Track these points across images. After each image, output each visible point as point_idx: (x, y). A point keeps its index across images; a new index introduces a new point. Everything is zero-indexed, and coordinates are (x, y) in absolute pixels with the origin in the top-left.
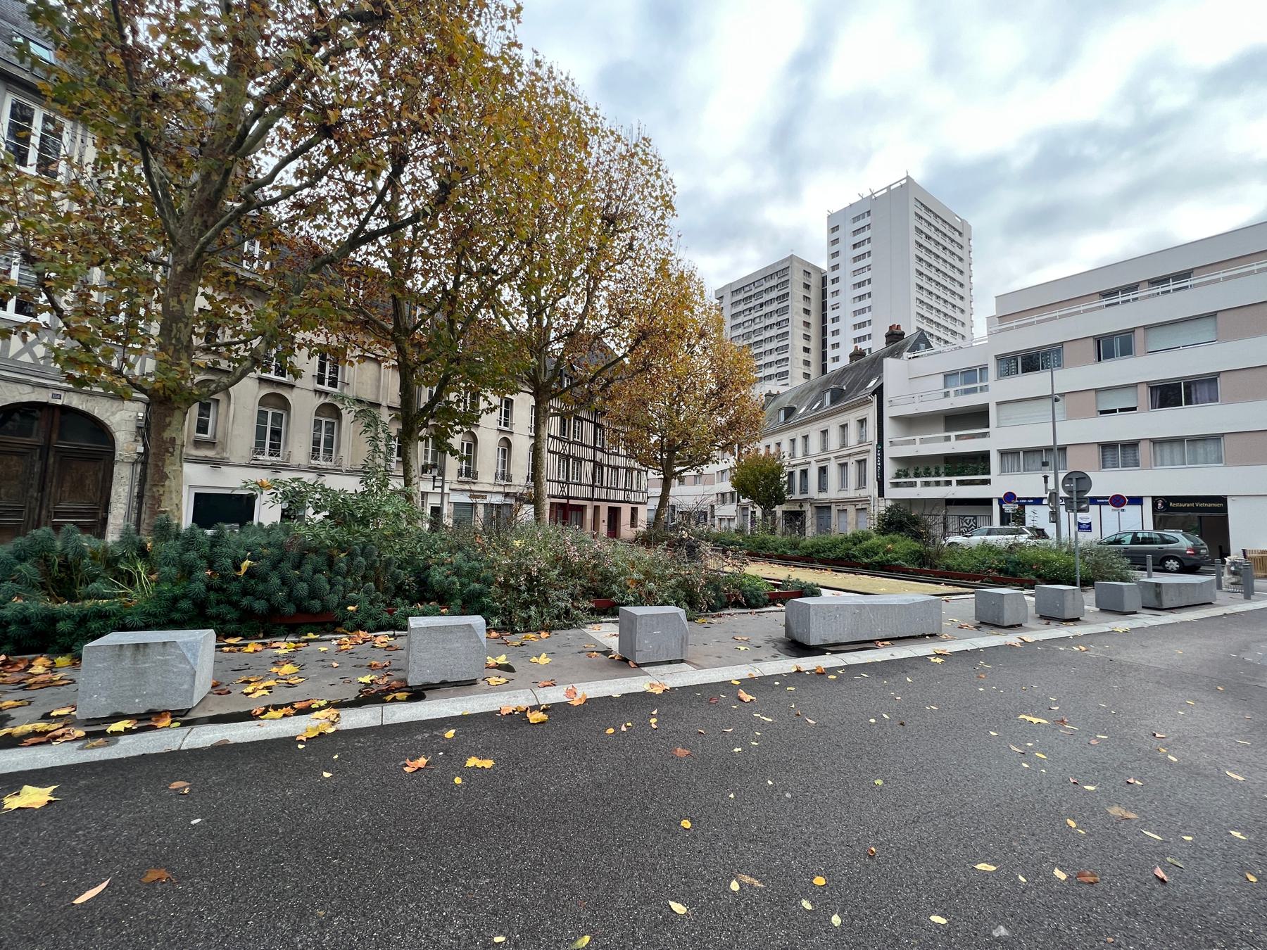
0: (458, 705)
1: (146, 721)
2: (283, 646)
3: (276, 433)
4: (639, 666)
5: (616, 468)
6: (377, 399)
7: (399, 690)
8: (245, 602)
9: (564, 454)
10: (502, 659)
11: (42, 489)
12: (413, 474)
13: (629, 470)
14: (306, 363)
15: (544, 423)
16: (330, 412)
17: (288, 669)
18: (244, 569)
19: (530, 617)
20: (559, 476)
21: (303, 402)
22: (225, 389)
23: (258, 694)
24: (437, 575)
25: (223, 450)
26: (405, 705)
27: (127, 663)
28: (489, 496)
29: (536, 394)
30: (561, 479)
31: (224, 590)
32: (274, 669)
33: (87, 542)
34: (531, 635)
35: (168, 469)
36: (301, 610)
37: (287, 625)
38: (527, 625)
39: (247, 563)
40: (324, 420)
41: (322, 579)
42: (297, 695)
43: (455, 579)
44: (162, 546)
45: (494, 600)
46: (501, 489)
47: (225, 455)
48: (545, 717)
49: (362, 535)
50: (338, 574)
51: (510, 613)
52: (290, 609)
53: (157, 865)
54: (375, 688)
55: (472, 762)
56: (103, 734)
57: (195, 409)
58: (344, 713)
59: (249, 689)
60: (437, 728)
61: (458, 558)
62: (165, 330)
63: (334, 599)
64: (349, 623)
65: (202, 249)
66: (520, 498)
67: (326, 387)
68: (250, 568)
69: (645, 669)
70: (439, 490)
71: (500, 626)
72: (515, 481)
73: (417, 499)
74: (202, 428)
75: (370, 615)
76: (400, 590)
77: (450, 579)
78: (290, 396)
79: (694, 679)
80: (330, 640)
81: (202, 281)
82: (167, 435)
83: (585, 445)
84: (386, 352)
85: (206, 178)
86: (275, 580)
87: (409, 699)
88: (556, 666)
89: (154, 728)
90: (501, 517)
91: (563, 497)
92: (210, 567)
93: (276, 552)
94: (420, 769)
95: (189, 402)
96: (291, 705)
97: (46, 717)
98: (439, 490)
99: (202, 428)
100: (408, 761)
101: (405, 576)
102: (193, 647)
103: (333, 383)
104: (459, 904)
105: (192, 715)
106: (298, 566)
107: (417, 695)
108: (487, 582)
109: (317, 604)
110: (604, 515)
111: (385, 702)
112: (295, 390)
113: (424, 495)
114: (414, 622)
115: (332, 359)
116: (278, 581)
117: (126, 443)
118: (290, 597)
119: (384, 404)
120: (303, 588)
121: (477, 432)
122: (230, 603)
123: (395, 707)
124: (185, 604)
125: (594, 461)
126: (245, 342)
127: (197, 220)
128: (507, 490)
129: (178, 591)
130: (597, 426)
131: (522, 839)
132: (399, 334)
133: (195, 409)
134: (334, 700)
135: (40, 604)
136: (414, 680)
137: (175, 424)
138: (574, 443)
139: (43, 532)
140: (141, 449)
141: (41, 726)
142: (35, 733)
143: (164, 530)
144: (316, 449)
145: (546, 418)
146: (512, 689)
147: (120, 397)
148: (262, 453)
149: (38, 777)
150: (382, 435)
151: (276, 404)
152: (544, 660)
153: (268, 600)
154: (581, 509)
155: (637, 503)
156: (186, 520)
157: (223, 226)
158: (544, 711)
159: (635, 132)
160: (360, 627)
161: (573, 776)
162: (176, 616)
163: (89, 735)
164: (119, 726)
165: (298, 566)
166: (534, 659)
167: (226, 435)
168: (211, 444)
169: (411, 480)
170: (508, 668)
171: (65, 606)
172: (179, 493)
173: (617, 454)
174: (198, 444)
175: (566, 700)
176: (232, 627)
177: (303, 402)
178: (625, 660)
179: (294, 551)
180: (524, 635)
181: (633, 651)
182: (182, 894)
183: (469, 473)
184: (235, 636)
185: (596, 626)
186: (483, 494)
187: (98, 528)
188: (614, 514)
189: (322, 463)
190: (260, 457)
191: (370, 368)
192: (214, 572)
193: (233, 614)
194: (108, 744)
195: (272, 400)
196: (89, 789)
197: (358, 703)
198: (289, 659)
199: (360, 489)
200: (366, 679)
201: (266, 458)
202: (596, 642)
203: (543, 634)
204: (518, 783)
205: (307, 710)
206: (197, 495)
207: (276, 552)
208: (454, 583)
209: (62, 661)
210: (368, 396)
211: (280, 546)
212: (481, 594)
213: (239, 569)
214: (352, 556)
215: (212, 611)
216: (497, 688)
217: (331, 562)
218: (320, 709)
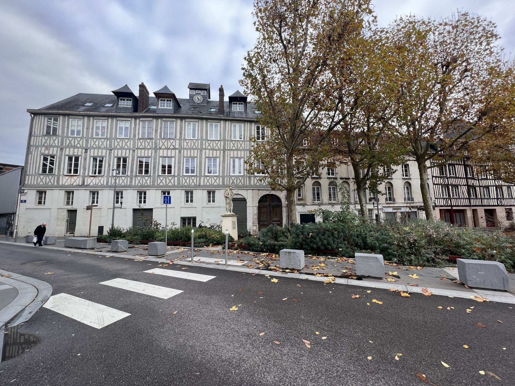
0: (374, 284)
1: (292, 270)
2: (322, 259)
3: (318, 194)
4: (471, 288)
5: (487, 187)
6: (348, 176)
7: (354, 276)
8: (311, 245)
9: (444, 184)
10: (395, 273)
11: (270, 215)
12: (363, 203)
13: (499, 187)
14: (324, 172)
15: (425, 172)
16: (332, 184)
17: (323, 265)
18: (310, 236)
19: (412, 260)
20: (443, 195)
21: (325, 182)
22: (303, 183)
23: (315, 270)
24: (369, 240)
25: (305, 201)
26: (355, 280)
27: (287, 256)
28: (402, 208)
29: (417, 160)
30: (445, 197)
31: (306, 241)
32: (319, 264)
33: (279, 228)
34: (412, 267)
35: (293, 208)
36: (326, 249)
37: (323, 253)
38: (411, 263)
39: (311, 234)
40: (331, 187)
41: (330, 239)
42: (325, 272)
43: (376, 242)
44: (292, 229)
45: (394, 251)
46: (408, 205)
47: (306, 202)
48: (409, 296)
49: (341, 225)
50: (335, 238)
51: (402, 257)
52: (323, 248)
53: (295, 298)
54: (347, 274)
55: (374, 301)
56: (285, 272)
57: (297, 190)
58: (336, 278)
59: (313, 268)
60: (365, 289)
61: (377, 234)
62: (288, 171)
63: (335, 246)
64: (340, 254)
65: (293, 148)
66: (420, 208)
67: (331, 176)
68: (312, 235)
69: (476, 290)
70: (376, 208)
71: (397, 261)
72: (416, 200)
73: (367, 212)
74: (299, 195)
75: (346, 252)
76: (357, 245)
77: (374, 241)
78: (321, 181)
79: (511, 301)
80: (335, 259)
81: (294, 155)
82: (291, 199)
83: (459, 178)
84: (347, 160)
85: (291, 128)
86: (318, 239)
87: (357, 279)
88: (421, 280)
89: (293, 272)
90: (408, 216)
91: (448, 206)
92: (303, 235)
93: (318, 231)
94: (356, 298)
95: (295, 189)
96: (323, 274)
97: (276, 266)
98: (376, 208)
99: (299, 195)
100: (353, 295)
101: (359, 241)
102: (299, 254)
103: (333, 174)
104: (361, 331)
105: (301, 272)
106: (323, 235)
107: (360, 278)
108: (391, 244)
109: (330, 247)
110: (481, 213)
111: (349, 278)
112: (322, 179)
113: (370, 210)
114: (356, 254)
115: (331, 167)
116: (319, 239)
117: (284, 202)
118: (322, 244)
119: (351, 178)
120: (325, 242)
121: (392, 182)
122: (308, 245)
123: (352, 280)
124: (298, 244)
125: (467, 185)
126: (305, 169)
127: (291, 140)
128: (412, 205)
129: (296, 241)
130: (466, 166)
131: (386, 325)
132: (351, 152)
133: (297, 190)
134: (334, 275)
135: (272, 242)
136: (359, 273)
137: (293, 196)
138: (450, 177)
139: (271, 225)
140: (287, 203)
141: (275, 268)
142: (274, 269)
143: (292, 225)
144: (330, 197)
145: (425, 171)
146: (397, 284)
147: (282, 191)
148: (315, 200)
149: (276, 277)
150: (346, 192)
151: (317, 184)
152: (415, 276)
153: (317, 245)
154: (463, 212)
155: (476, 206)
156: (298, 221)
157: (297, 138)
158: (409, 294)
159: (457, 14)
160: (343, 256)
161: (414, 315)
162: (297, 247)
163: (283, 271)
164: (287, 271)
165: (323, 235)
166: (410, 276)
167: (305, 196)
168: (302, 200)
169: (363, 205)
170: (398, 277)
171: (276, 243)
172: (295, 214)
173: (487, 179)
174: (299, 200)
175: (422, 292)
176: (309, 252)
177: (325, 182)
178: (463, 284)
179: (322, 231)
180: (408, 267)
181: (466, 280)
182: (299, 305)
183: (391, 199)
184: (310, 254)
185: (451, 268)
186: (399, 208)
187: (281, 225)
188: (490, 213)
189: (333, 202)
190: (315, 202)
191: (343, 166)
192: (303, 236)
193: (309, 248)
194: (286, 274)
195: (316, 184)
196: (283, 282)
197: (341, 277)
198: (324, 262)
199: (341, 210)
200: (344, 271)
201: (316, 202)
202: (448, 275)
203: (419, 268)
204: (390, 311)
205: (327, 276)
206: (301, 215)
207: (318, 231)
208: (376, 243)
209: (277, 255)
210: (345, 176)
211: (318, 229)
212: (387, 248)
213: (309, 236)
214: (339, 233)
215: (304, 247)
216: (391, 282)
217: (333, 234)
218: (330, 276)
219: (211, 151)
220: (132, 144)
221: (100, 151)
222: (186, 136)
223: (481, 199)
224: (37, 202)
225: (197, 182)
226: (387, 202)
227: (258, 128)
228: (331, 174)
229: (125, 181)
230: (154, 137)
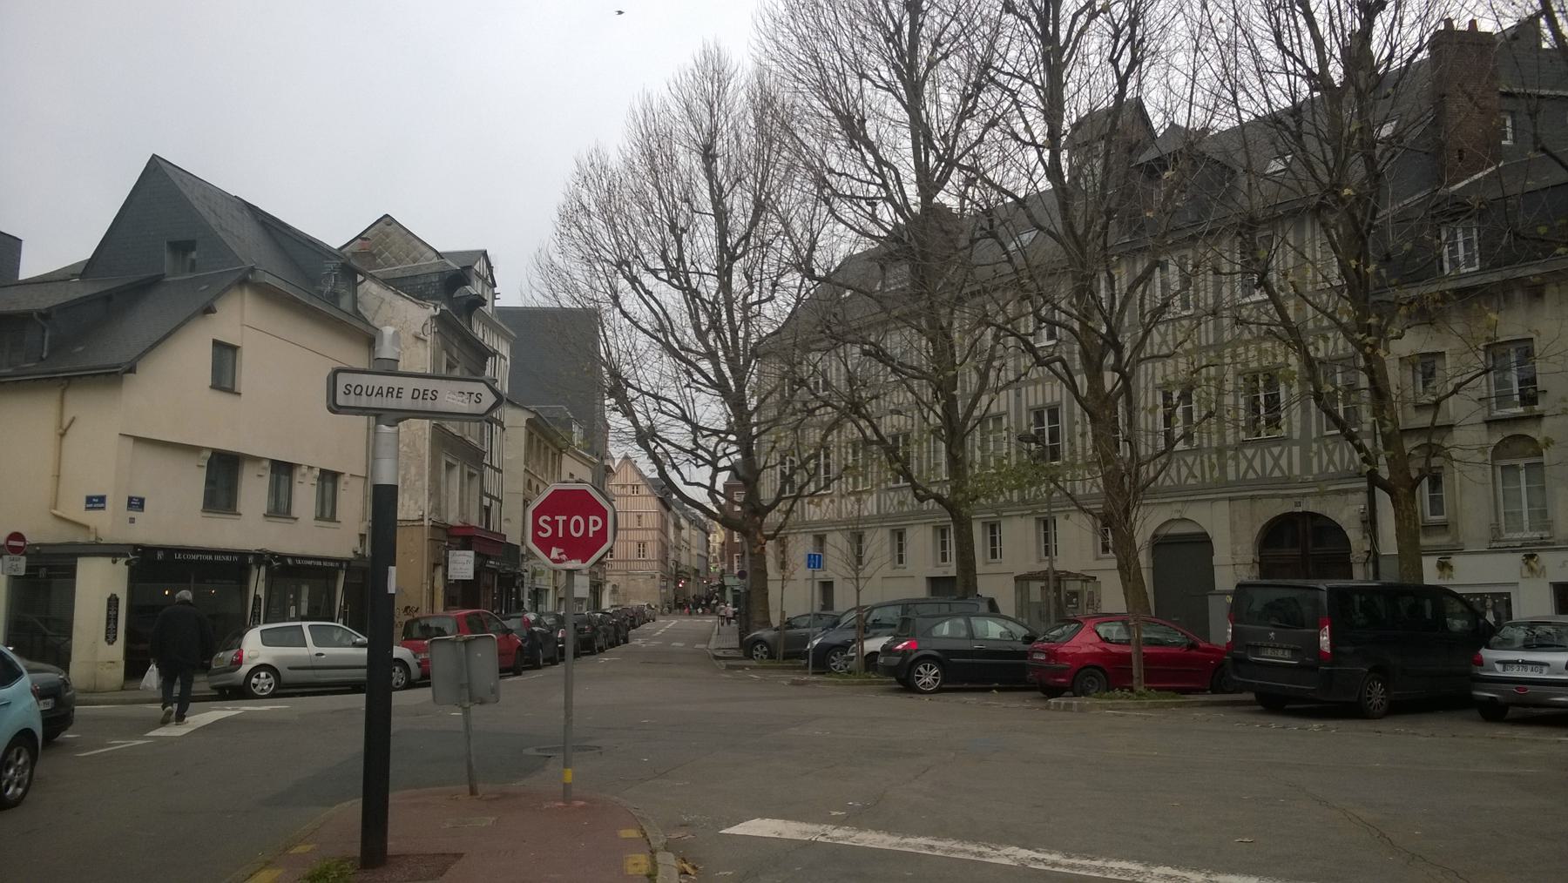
225: (885, 500)
229: (1284, 462)
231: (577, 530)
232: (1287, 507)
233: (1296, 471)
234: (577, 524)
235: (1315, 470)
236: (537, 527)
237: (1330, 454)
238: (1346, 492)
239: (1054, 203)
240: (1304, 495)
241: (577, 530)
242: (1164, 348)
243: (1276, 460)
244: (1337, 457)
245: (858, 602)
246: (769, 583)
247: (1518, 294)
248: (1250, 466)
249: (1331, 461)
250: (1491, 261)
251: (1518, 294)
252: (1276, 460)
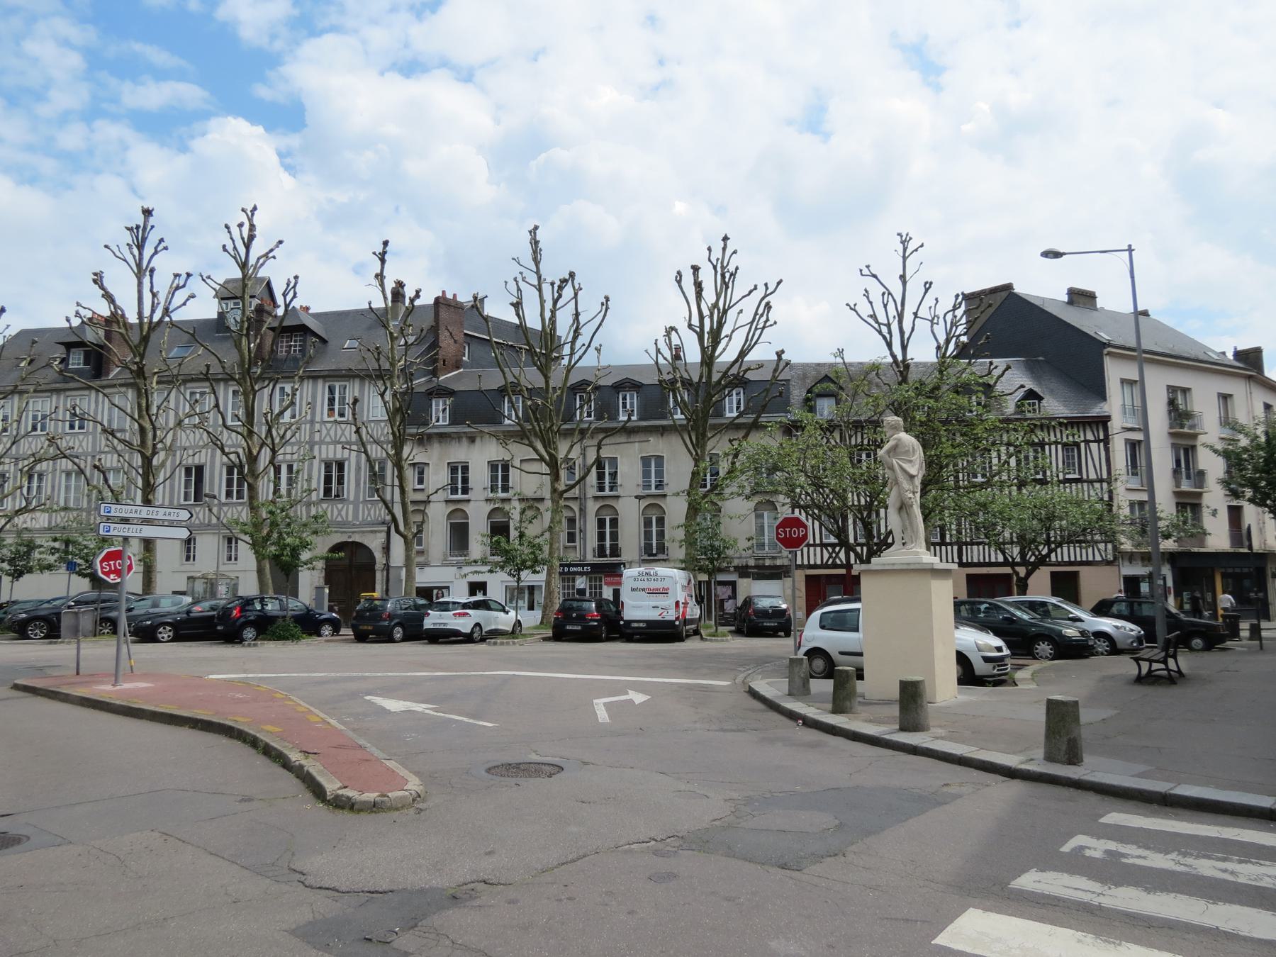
78: (468, 508)
91: (835, 566)
112: (472, 503)
219: (331, 447)
220: (90, 445)
221: (324, 447)
222: (371, 414)
223: (960, 544)
224: (184, 559)
225: (204, 518)
226: (642, 558)
227: (331, 391)
228: (460, 491)
229: (343, 513)
230: (128, 428)
231: (795, 534)
232: (344, 538)
233: (350, 519)
234: (795, 531)
235: (361, 519)
236: (778, 534)
237: (369, 510)
238: (376, 532)
239: (223, 289)
240: (353, 532)
241: (795, 534)
242: (328, 437)
243: (340, 512)
244: (372, 512)
245: (68, 593)
246: (256, 569)
247: (464, 439)
248: (339, 514)
249: (369, 514)
250: (454, 421)
251: (464, 439)
252: (340, 512)
